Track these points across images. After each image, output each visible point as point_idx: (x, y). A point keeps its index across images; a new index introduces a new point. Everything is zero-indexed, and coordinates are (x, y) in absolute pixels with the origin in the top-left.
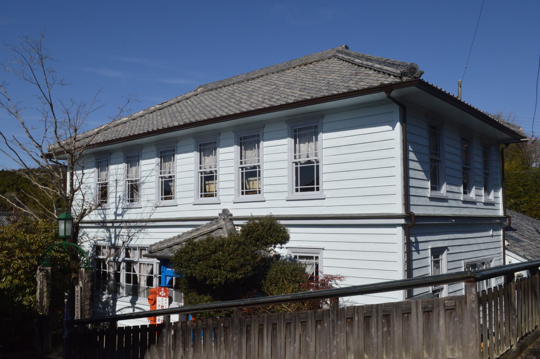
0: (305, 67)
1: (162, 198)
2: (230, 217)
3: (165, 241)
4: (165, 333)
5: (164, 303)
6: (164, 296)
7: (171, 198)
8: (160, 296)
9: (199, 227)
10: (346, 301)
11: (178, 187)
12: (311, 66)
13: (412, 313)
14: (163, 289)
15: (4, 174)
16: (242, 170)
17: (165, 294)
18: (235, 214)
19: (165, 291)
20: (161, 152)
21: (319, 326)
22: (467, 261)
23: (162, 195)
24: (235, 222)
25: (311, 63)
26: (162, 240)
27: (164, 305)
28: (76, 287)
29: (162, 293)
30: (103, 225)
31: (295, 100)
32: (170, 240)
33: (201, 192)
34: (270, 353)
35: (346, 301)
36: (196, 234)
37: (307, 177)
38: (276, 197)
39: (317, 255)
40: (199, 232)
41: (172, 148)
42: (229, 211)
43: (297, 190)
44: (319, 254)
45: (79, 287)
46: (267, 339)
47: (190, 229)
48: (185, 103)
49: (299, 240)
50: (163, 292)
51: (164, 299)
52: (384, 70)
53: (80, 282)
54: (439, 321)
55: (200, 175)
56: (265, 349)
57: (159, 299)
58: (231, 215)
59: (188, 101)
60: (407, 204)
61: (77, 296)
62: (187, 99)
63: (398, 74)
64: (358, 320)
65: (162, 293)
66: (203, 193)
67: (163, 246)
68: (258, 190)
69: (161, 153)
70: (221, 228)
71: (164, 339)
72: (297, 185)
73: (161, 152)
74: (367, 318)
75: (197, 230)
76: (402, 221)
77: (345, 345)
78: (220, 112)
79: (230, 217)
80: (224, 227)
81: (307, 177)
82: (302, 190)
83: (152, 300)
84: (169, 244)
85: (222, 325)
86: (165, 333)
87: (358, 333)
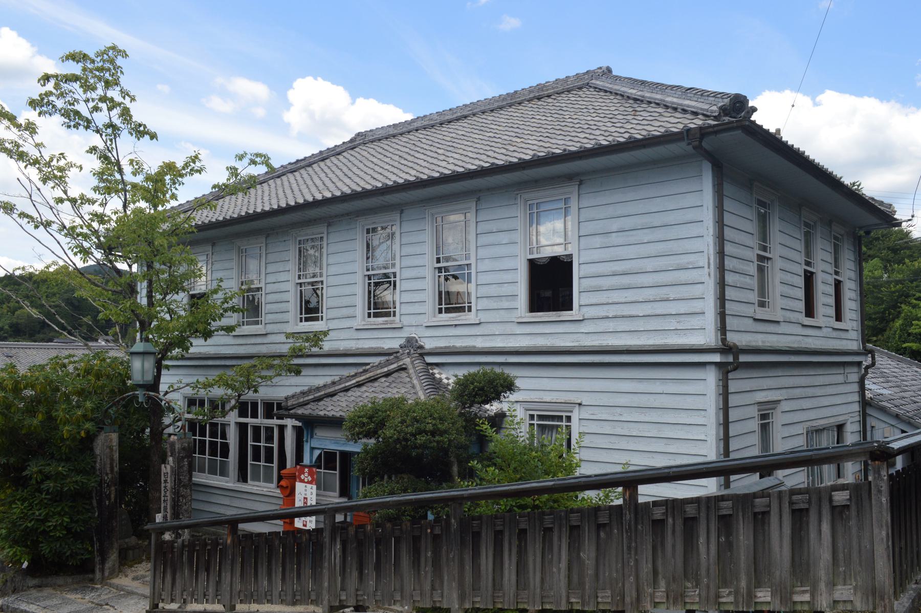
0: (540, 103)
1: (301, 319)
2: (419, 351)
3: (310, 391)
4: (327, 545)
5: (308, 493)
6: (308, 482)
7: (317, 319)
8: (302, 481)
9: (368, 367)
10: (647, 493)
11: (330, 299)
12: (550, 100)
13: (772, 513)
14: (306, 470)
15: (10, 280)
16: (370, 279)
17: (310, 479)
18: (429, 345)
19: (310, 474)
20: (300, 241)
21: (602, 534)
22: (809, 424)
23: (301, 314)
24: (429, 359)
25: (549, 96)
26: (306, 388)
27: (309, 496)
28: (163, 466)
29: (306, 476)
30: (736, 358)
31: (534, 155)
32: (318, 389)
33: (369, 309)
34: (514, 577)
35: (647, 493)
36: (362, 378)
37: (550, 284)
38: (501, 318)
39: (568, 414)
40: (368, 376)
41: (320, 236)
42: (417, 341)
43: (440, 311)
44: (571, 412)
45: (168, 467)
46: (510, 555)
47: (353, 371)
48: (336, 161)
49: (531, 391)
50: (306, 475)
51: (309, 486)
52: (685, 105)
53: (171, 459)
54: (820, 525)
55: (367, 281)
56: (506, 573)
57: (299, 486)
58: (421, 347)
59: (340, 157)
60: (723, 329)
61: (166, 481)
62: (339, 154)
63: (712, 112)
64: (674, 524)
65: (306, 476)
66: (372, 311)
67: (306, 398)
68: (466, 305)
69: (300, 243)
70: (405, 369)
71: (326, 553)
72: (440, 304)
73: (300, 241)
74: (690, 524)
75: (365, 371)
76: (717, 358)
77: (650, 566)
78: (362, 184)
79: (419, 351)
80: (410, 367)
81: (550, 284)
82: (307, 320)
83: (287, 487)
84: (316, 395)
85: (429, 531)
86: (327, 545)
87: (674, 546)
